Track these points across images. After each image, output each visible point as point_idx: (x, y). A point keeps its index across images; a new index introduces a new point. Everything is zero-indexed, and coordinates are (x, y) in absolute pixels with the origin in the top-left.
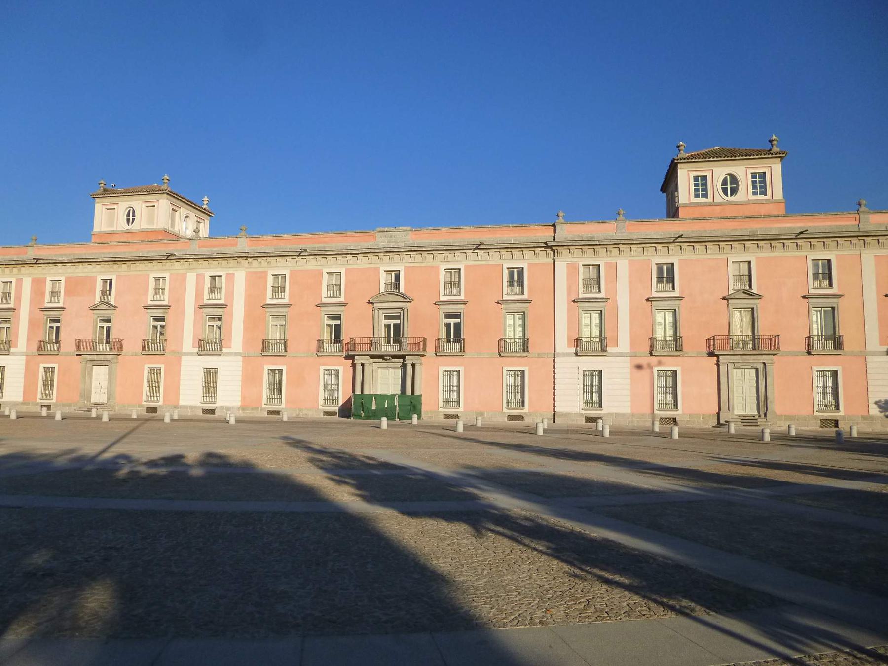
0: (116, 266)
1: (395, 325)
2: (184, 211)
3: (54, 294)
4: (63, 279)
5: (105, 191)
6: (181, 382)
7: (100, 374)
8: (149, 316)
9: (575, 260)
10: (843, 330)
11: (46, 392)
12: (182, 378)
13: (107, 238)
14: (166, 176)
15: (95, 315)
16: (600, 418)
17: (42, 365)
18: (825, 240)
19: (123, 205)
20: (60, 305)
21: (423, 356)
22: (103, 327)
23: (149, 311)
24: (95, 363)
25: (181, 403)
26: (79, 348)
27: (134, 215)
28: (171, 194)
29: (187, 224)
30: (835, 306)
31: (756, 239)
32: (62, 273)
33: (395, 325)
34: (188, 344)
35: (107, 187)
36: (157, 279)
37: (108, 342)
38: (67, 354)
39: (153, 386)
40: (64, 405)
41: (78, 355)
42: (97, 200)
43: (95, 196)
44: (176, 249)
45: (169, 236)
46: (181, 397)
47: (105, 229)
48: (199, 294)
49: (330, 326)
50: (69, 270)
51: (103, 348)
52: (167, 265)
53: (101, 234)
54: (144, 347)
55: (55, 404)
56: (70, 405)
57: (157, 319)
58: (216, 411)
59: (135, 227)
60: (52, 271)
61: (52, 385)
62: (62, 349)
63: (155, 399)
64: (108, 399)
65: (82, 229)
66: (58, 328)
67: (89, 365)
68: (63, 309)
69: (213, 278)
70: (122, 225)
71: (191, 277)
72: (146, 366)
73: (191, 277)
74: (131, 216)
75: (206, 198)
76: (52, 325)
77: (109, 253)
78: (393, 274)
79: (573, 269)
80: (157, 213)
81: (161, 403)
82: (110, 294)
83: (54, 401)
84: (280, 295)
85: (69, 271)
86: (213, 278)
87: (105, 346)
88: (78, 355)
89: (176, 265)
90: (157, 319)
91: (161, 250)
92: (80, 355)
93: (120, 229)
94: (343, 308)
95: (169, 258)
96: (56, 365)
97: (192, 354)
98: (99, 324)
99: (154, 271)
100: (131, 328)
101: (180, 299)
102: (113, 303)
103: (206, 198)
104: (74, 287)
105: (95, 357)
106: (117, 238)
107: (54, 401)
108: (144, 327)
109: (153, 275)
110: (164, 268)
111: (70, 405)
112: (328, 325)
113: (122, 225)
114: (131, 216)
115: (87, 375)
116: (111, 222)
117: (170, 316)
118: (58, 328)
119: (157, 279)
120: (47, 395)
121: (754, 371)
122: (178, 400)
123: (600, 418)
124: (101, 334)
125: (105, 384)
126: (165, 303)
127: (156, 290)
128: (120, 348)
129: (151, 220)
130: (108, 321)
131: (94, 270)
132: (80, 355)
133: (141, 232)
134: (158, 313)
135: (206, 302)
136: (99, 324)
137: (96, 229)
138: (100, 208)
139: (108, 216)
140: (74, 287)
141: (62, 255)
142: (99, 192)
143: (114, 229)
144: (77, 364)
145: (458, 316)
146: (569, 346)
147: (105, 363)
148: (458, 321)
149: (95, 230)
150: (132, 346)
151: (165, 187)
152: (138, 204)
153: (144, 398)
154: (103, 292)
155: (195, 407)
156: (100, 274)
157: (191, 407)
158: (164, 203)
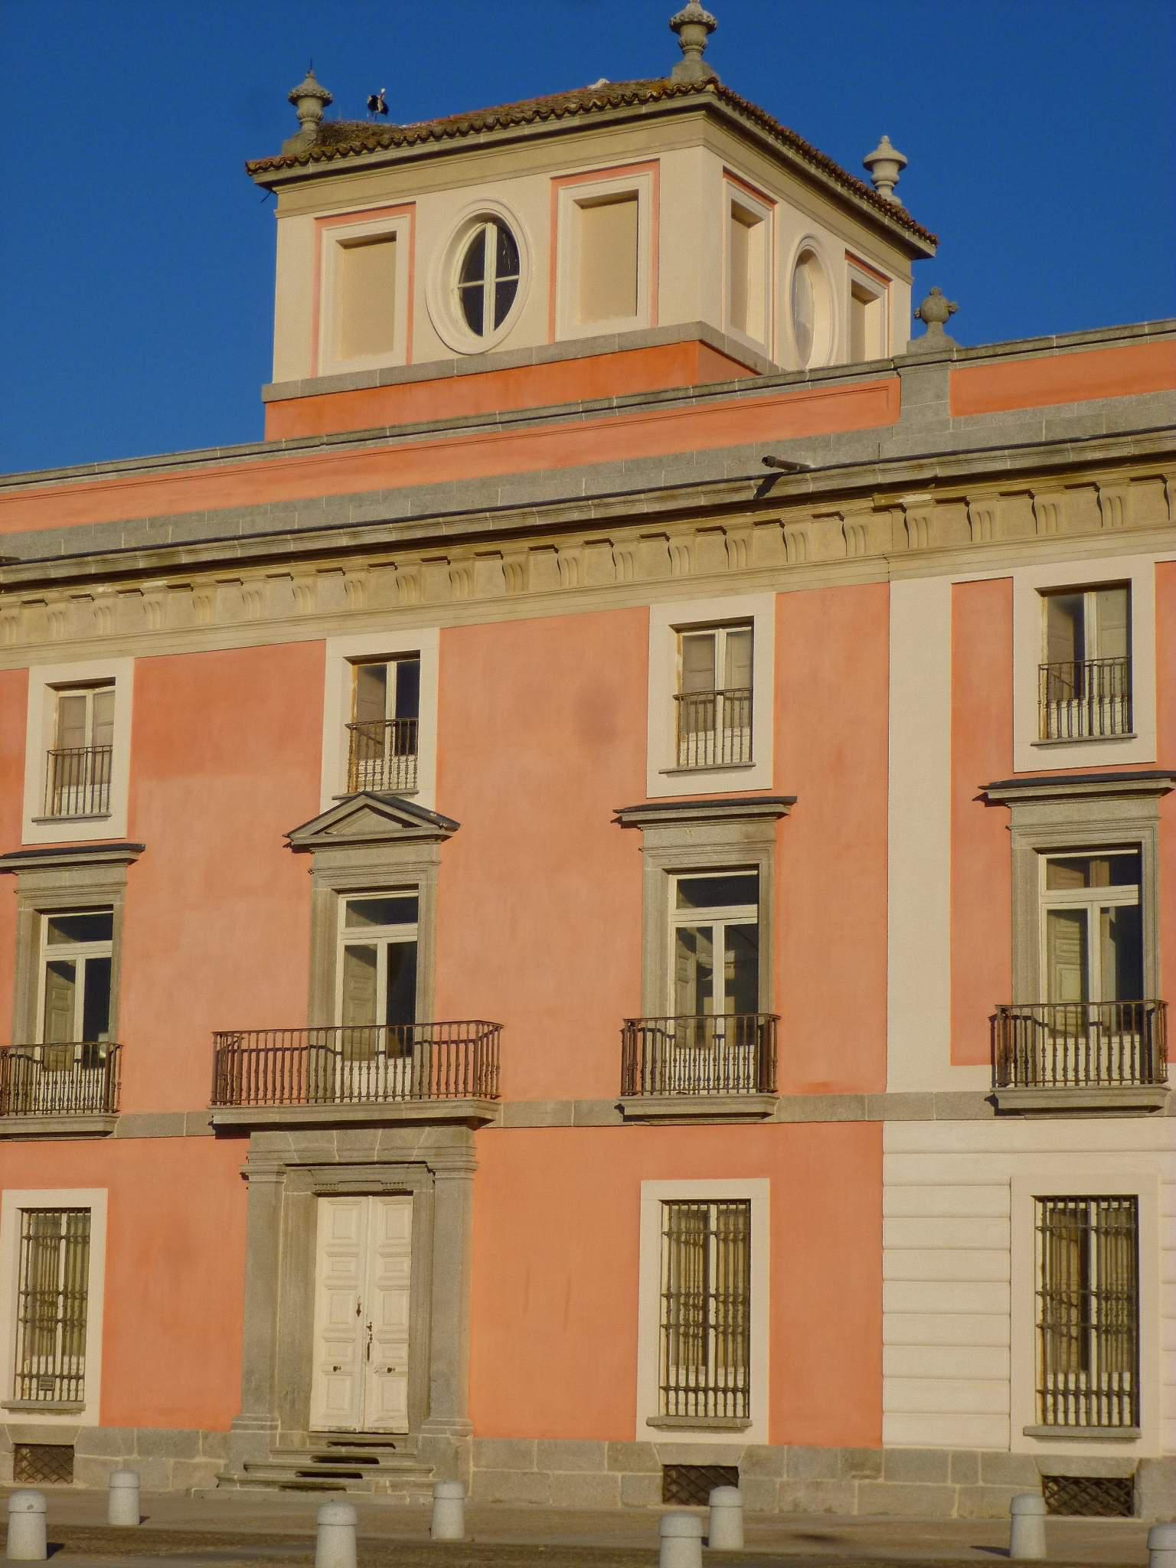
0: (436, 574)
1: (91, 964)
2: (789, 221)
3: (71, 763)
4: (124, 672)
5: (329, 136)
6: (892, 1297)
7: (361, 1245)
8: (652, 869)
9: (977, 567)
10: (783, 989)
11: (40, 1365)
12: (892, 1264)
13: (365, 415)
14: (309, 85)
15: (317, 886)
16: (728, 1476)
17: (654, 1192)
18: (842, 506)
19: (435, 214)
20: (113, 829)
21: (476, 1123)
22: (1079, 916)
23: (653, 836)
24: (331, 1182)
25: (897, 1434)
26: (224, 1090)
27: (509, 259)
28: (736, 117)
29: (809, 299)
30: (1145, 837)
31: (432, 541)
32: (112, 640)
33: (91, 964)
34: (924, 1043)
35: (341, 118)
36: (696, 635)
37: (402, 1044)
38: (164, 1128)
39: (707, 1322)
40: (147, 1446)
41: (225, 1131)
42: (286, 197)
43: (272, 179)
44: (816, 439)
45: (714, 367)
46: (892, 1396)
47: (337, 362)
48: (976, 717)
49: (363, 954)
50: (160, 608)
51: (376, 1080)
52: (758, 539)
53: (317, 395)
54: (629, 1071)
55: (99, 1441)
56: (183, 1446)
57: (700, 891)
58: (1146, 1493)
59: (520, 332)
60: (59, 630)
61: (76, 1324)
62: (132, 1101)
63: (724, 1406)
64: (421, 1407)
65: (203, 360)
66: (99, 970)
67: (294, 1190)
68: (127, 852)
69: (1066, 601)
70: (444, 335)
71: (921, 613)
72: (654, 1192)
73: (921, 613)
74: (490, 275)
75: (886, 149)
76: (1072, 897)
77: (388, 495)
78: (392, 668)
79: (979, 608)
80: (673, 244)
81: (758, 1433)
82: (407, 744)
83: (90, 1417)
84: (720, 743)
85: (155, 621)
86: (1066, 601)
87: (382, 1076)
88: (225, 1131)
89: (814, 535)
90: (700, 891)
91: (721, 446)
92: (240, 1131)
93: (428, 352)
94: (116, 873)
95: (772, 494)
96: (95, 1199)
97: (950, 1107)
98: (347, 934)
99: (674, 590)
100: (551, 955)
101: (856, 757)
102: (426, 799)
103: (886, 149)
104: (189, 719)
105: (331, 1144)
106: (418, 407)
107: (90, 1417)
108: (634, 943)
109: (669, 611)
110: (740, 560)
111: (183, 1446)
112: (686, 938)
113: (444, 335)
114: (490, 275)
115: (283, 1259)
116: (371, 318)
117: (792, 870)
118: (99, 970)
119: (696, 635)
120: (46, 1382)
121: (323, 1201)
122: (875, 1410)
123: (728, 1476)
124: (57, 1007)
125: (392, 1311)
126: (759, 780)
127: (696, 707)
128: (483, 1078)
129: (616, 277)
130: (404, 911)
131: (307, 605)
132: (240, 1131)
133: (558, 361)
134: (715, 846)
135: (1029, 760)
136: (347, 934)
137: (289, 366)
138: (306, 245)
139: (353, 287)
140: (189, 719)
141: (112, 527)
142: (296, 147)
143: (395, 358)
144: (217, 1187)
145: (740, 888)
146: (956, 1061)
147: (395, 1176)
148: (1125, 895)
149: (277, 378)
150: (560, 1063)
151: (691, 69)
152: (531, 193)
153: (649, 1401)
154: (363, 737)
155: (994, 1462)
156: (338, 625)
157: (965, 1463)
158: (687, 172)
